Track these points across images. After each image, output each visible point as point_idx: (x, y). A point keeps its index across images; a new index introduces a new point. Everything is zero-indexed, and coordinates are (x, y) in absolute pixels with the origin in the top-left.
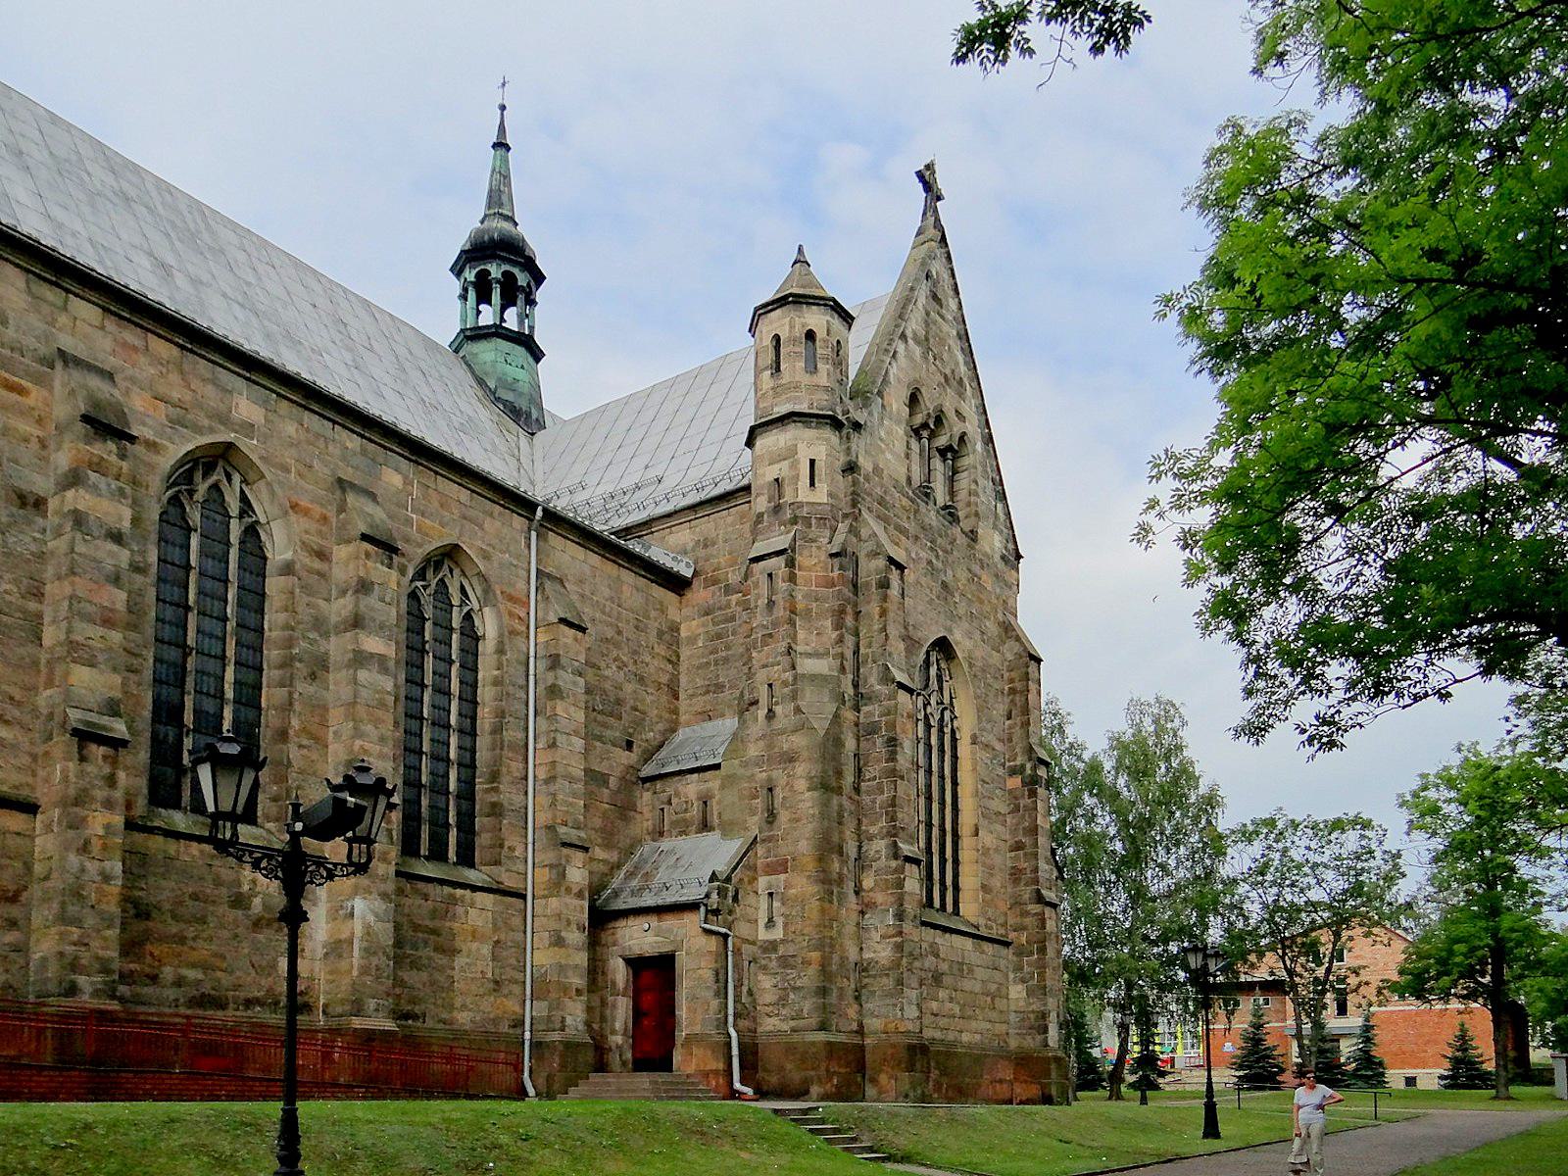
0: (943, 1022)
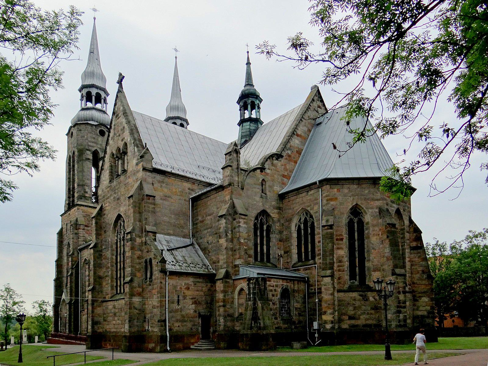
0: (116, 326)
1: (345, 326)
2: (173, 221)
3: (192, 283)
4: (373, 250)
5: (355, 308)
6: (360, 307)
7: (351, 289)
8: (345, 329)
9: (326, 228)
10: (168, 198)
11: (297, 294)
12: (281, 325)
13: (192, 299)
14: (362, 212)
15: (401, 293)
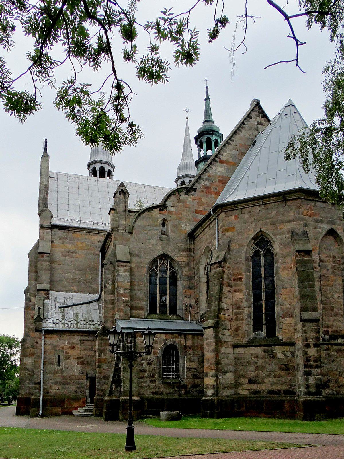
1: (243, 392)
2: (77, 277)
3: (79, 342)
4: (282, 290)
5: (257, 368)
6: (264, 367)
7: (251, 344)
8: (245, 396)
9: (215, 266)
10: (71, 254)
11: (190, 352)
12: (162, 390)
13: (78, 358)
14: (270, 241)
15: (312, 346)
